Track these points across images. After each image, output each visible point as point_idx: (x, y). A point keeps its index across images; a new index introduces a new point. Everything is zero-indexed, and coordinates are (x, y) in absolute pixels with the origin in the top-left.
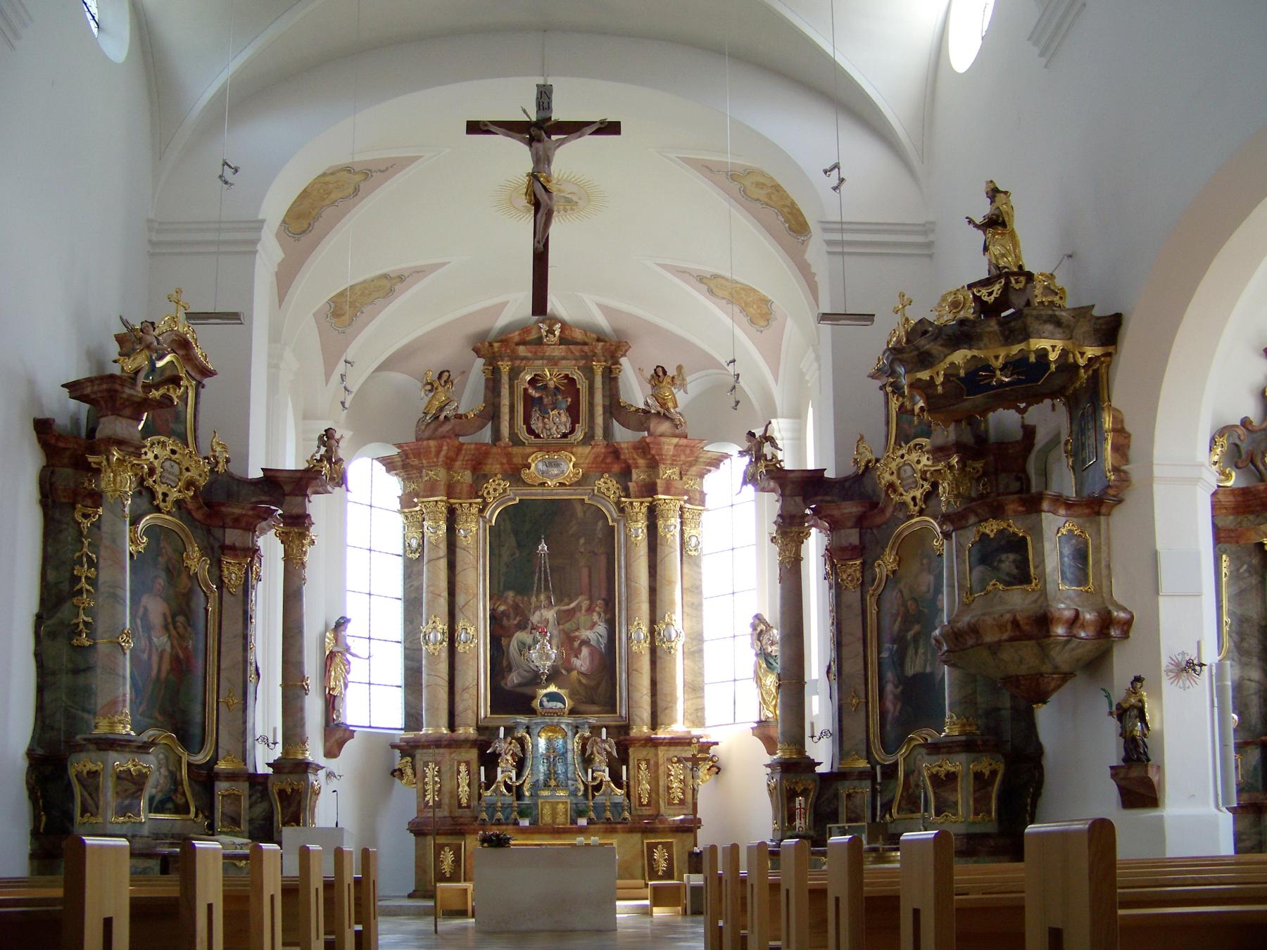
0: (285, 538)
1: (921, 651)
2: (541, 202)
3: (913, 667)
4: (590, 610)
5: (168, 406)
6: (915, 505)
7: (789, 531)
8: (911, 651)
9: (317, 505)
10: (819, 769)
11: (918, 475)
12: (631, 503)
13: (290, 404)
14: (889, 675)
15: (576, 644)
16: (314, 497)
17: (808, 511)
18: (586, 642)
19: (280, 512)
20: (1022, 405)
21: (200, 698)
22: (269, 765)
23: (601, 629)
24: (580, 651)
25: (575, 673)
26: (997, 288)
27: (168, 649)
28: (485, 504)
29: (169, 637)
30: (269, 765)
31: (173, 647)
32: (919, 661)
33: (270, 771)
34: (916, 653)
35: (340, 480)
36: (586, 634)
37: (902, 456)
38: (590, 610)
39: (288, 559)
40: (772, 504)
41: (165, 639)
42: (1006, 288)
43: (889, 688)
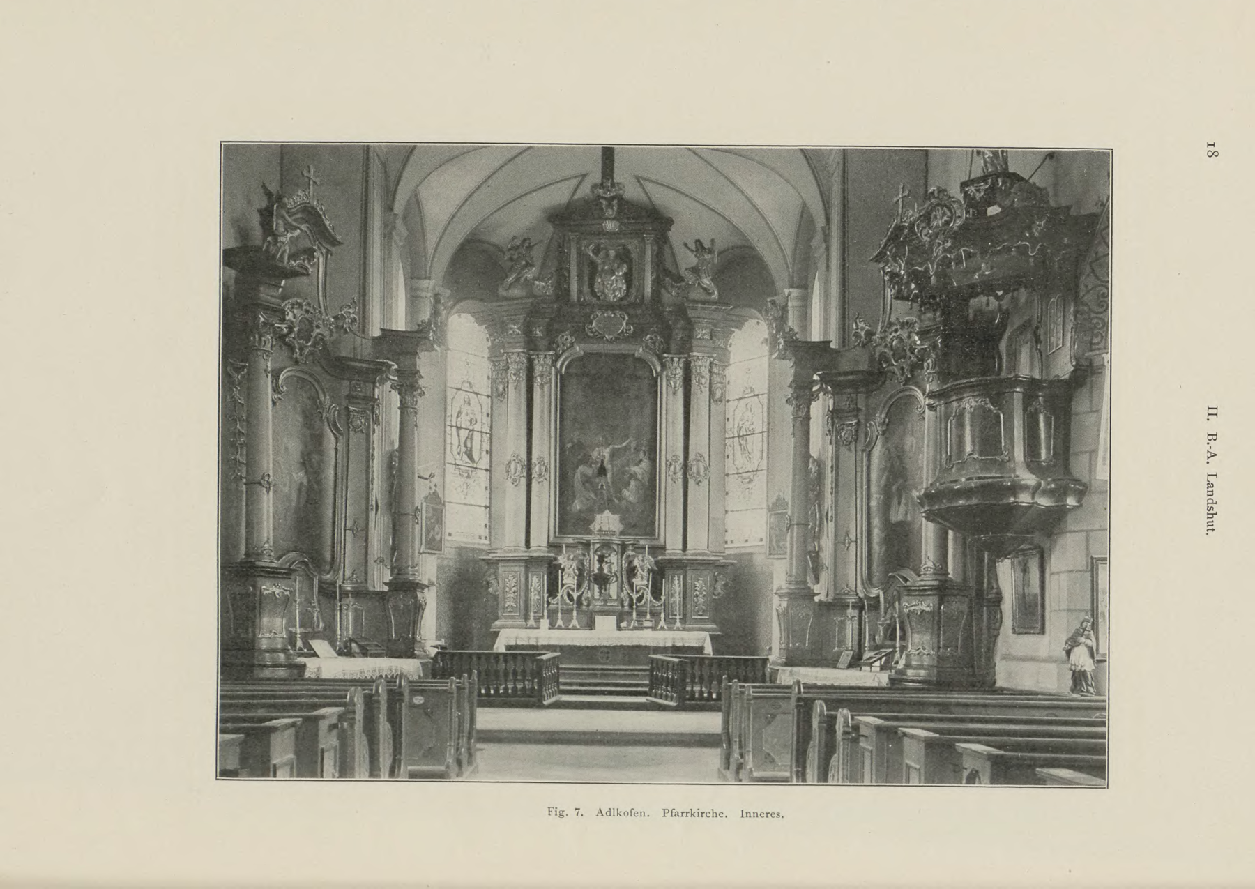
0: (399, 388)
1: (903, 501)
2: (1087, 541)
3: (897, 515)
4: (637, 450)
5: (303, 274)
6: (903, 374)
7: (802, 394)
8: (895, 501)
9: (424, 362)
10: (816, 599)
11: (907, 348)
12: (672, 359)
13: (401, 272)
14: (876, 521)
15: (626, 477)
16: (421, 354)
17: (815, 377)
18: (633, 476)
19: (396, 367)
20: (1000, 293)
21: (329, 542)
22: (386, 584)
23: (645, 464)
24: (629, 484)
25: (624, 502)
26: (983, 186)
27: (305, 481)
28: (558, 357)
29: (306, 472)
30: (386, 584)
31: (309, 481)
32: (902, 509)
33: (386, 589)
34: (899, 503)
35: (441, 340)
36: (634, 469)
37: (896, 331)
38: (637, 450)
39: (403, 408)
40: (787, 368)
41: (301, 474)
42: (993, 188)
43: (876, 532)
